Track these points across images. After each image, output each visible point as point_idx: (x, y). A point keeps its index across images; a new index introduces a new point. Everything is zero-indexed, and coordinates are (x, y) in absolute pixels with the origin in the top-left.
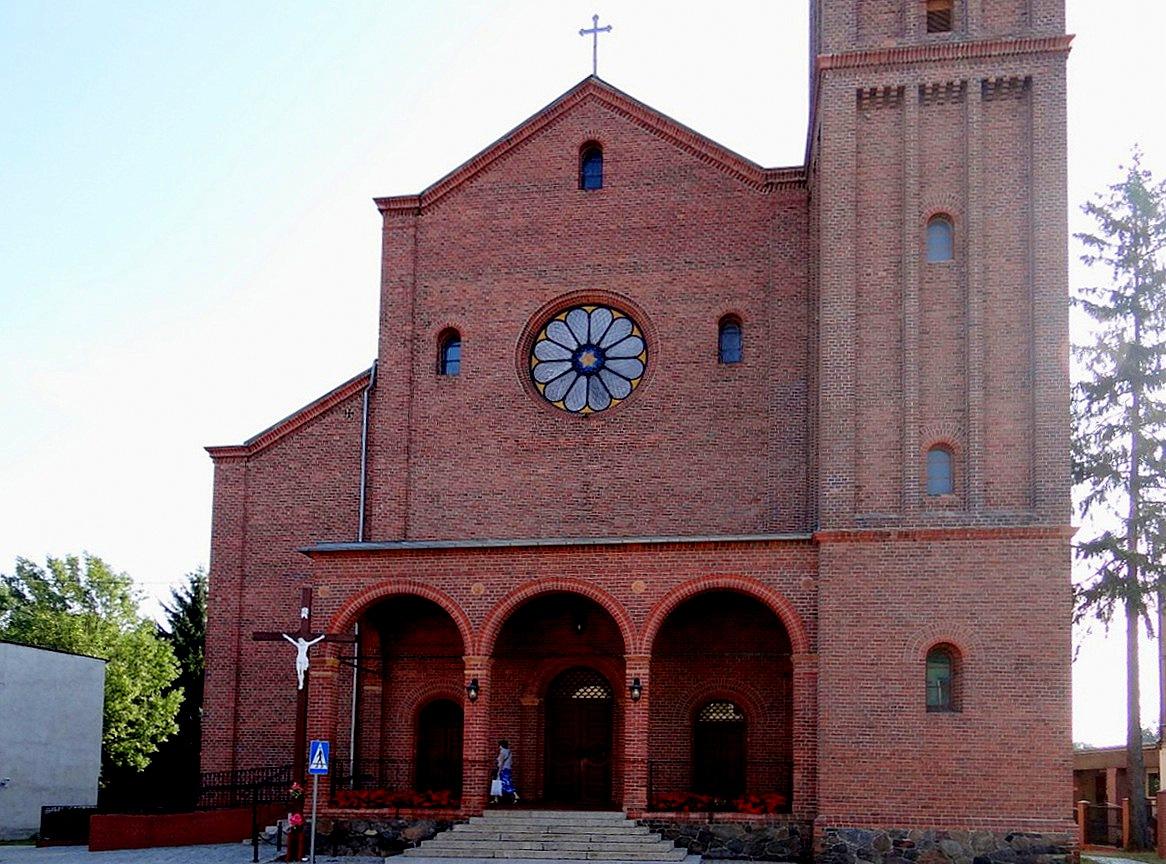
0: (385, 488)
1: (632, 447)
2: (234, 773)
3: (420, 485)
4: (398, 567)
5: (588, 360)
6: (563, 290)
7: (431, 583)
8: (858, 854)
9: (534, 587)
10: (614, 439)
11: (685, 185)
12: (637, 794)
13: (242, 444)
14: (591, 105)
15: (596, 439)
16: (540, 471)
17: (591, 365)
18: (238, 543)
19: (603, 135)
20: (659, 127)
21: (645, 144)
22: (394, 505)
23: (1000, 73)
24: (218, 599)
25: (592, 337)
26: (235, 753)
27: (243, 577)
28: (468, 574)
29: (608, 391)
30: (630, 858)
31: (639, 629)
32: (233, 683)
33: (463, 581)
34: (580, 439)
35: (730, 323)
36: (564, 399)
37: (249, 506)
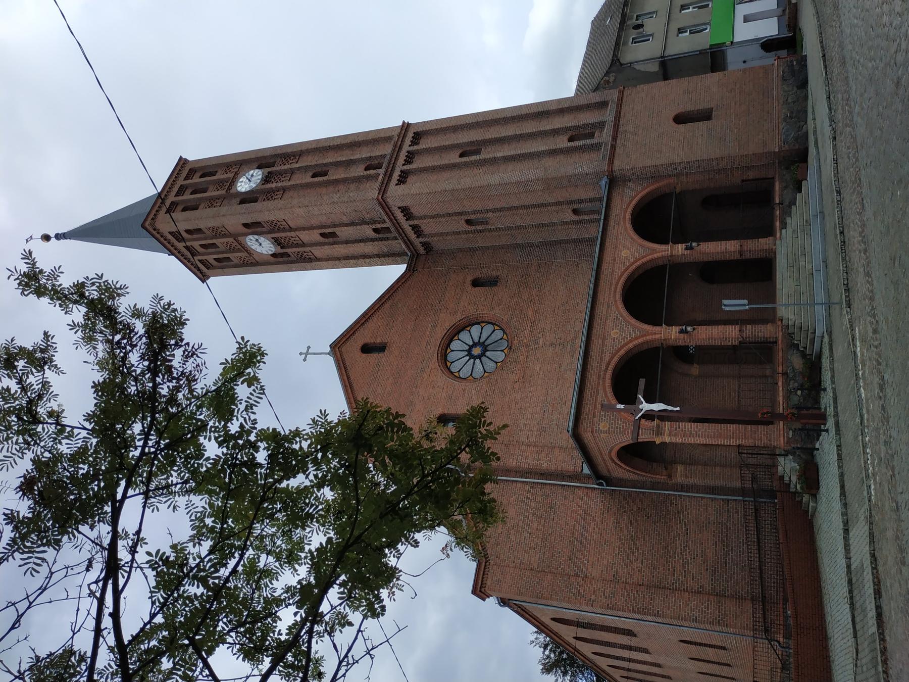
0: (530, 460)
1: (534, 323)
2: (743, 492)
3: (532, 438)
4: (592, 377)
5: (477, 351)
6: (435, 359)
7: (607, 359)
8: (798, 131)
9: (618, 304)
10: (527, 332)
11: (400, 306)
12: (763, 243)
13: (474, 564)
14: (343, 349)
15: (525, 341)
16: (538, 369)
17: (480, 349)
18: (549, 577)
19: (360, 343)
20: (367, 317)
21: (371, 325)
22: (543, 454)
23: (409, 141)
24: (593, 597)
25: (465, 349)
26: (732, 597)
27: (577, 575)
28: (604, 339)
29: (498, 340)
30: (808, 204)
31: (654, 251)
32: (667, 592)
33: (608, 342)
34: (523, 349)
35: (476, 283)
36: (496, 363)
37: (522, 566)
